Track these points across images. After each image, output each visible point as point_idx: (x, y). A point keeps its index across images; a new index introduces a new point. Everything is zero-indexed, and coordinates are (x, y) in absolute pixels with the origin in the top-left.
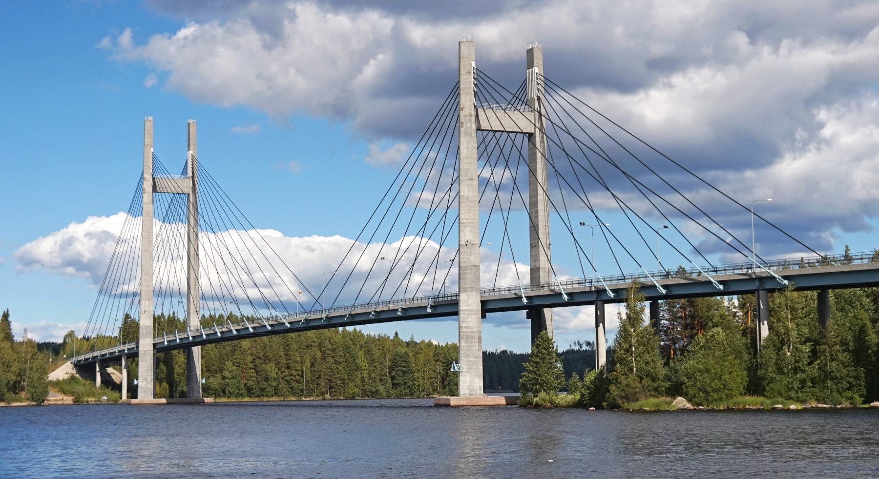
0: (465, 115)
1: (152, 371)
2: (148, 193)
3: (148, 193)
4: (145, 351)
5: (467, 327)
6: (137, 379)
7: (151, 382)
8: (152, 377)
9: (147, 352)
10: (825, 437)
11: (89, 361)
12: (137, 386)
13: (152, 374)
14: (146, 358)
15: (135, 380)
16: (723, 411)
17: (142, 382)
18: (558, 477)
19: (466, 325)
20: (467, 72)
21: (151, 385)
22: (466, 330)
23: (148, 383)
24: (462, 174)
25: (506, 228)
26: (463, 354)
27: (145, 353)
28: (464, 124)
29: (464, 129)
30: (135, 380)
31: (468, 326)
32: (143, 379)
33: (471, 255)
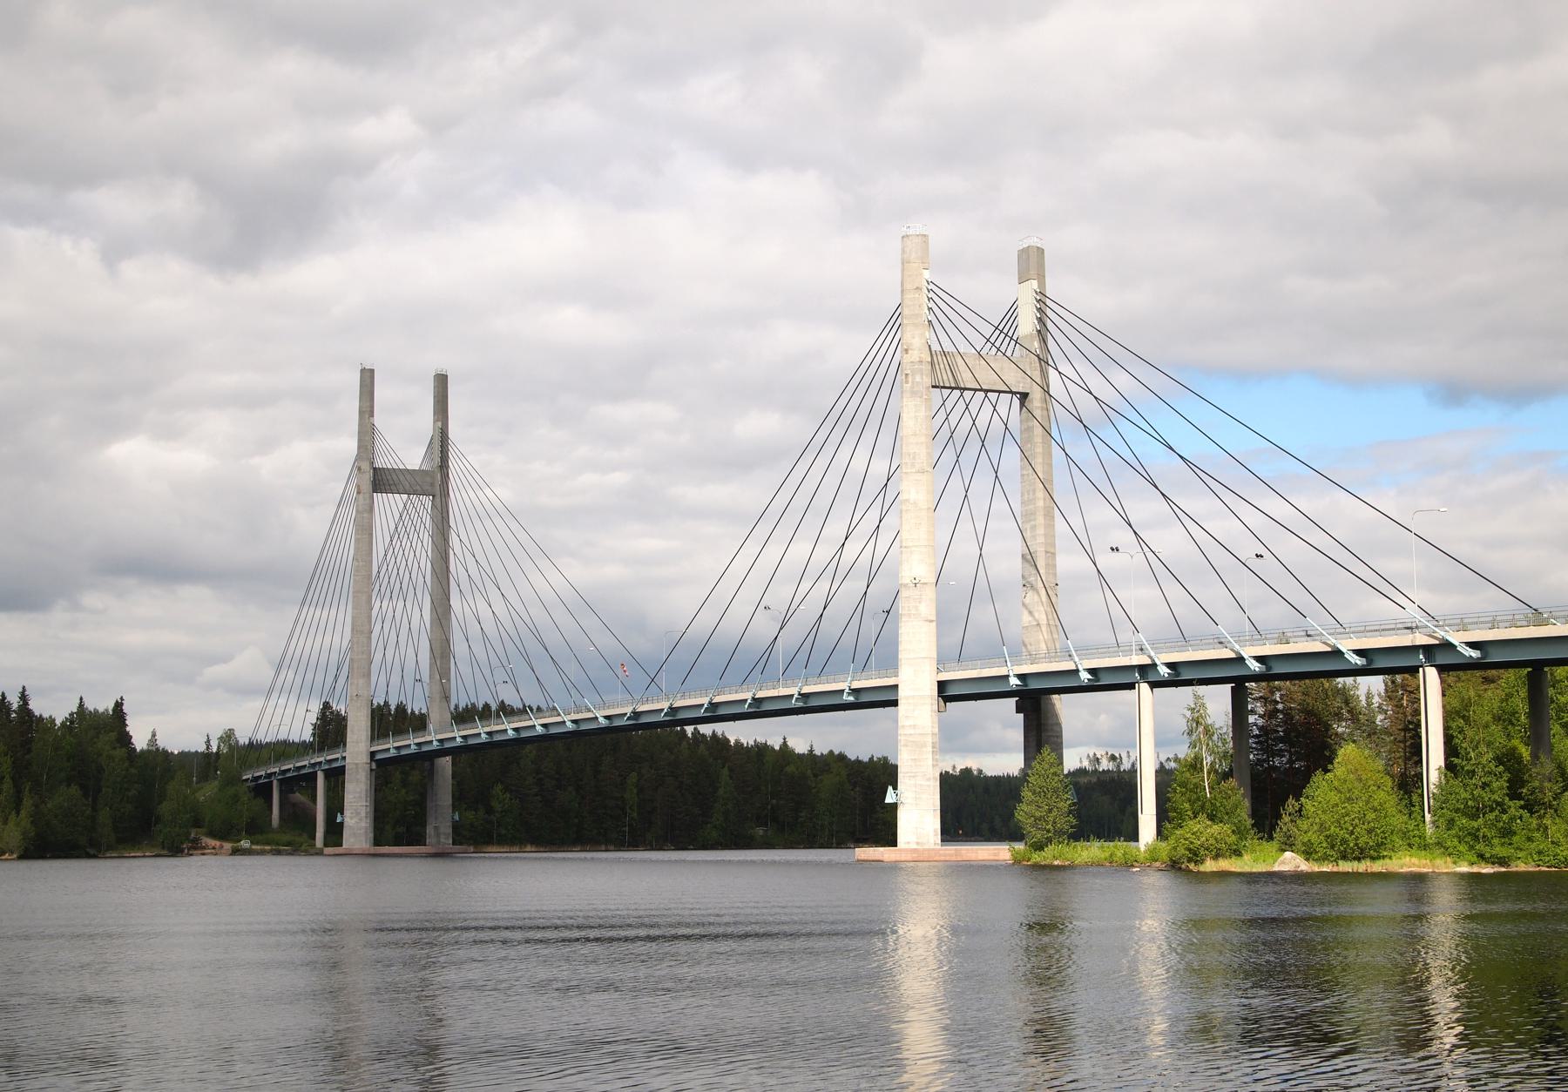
0: (912, 362)
4: (357, 764)
5: (914, 727)
9: (360, 766)
12: (894, 806)
17: (351, 818)
22: (912, 732)
23: (360, 820)
27: (357, 768)
31: (915, 725)
32: (352, 813)
33: (920, 602)
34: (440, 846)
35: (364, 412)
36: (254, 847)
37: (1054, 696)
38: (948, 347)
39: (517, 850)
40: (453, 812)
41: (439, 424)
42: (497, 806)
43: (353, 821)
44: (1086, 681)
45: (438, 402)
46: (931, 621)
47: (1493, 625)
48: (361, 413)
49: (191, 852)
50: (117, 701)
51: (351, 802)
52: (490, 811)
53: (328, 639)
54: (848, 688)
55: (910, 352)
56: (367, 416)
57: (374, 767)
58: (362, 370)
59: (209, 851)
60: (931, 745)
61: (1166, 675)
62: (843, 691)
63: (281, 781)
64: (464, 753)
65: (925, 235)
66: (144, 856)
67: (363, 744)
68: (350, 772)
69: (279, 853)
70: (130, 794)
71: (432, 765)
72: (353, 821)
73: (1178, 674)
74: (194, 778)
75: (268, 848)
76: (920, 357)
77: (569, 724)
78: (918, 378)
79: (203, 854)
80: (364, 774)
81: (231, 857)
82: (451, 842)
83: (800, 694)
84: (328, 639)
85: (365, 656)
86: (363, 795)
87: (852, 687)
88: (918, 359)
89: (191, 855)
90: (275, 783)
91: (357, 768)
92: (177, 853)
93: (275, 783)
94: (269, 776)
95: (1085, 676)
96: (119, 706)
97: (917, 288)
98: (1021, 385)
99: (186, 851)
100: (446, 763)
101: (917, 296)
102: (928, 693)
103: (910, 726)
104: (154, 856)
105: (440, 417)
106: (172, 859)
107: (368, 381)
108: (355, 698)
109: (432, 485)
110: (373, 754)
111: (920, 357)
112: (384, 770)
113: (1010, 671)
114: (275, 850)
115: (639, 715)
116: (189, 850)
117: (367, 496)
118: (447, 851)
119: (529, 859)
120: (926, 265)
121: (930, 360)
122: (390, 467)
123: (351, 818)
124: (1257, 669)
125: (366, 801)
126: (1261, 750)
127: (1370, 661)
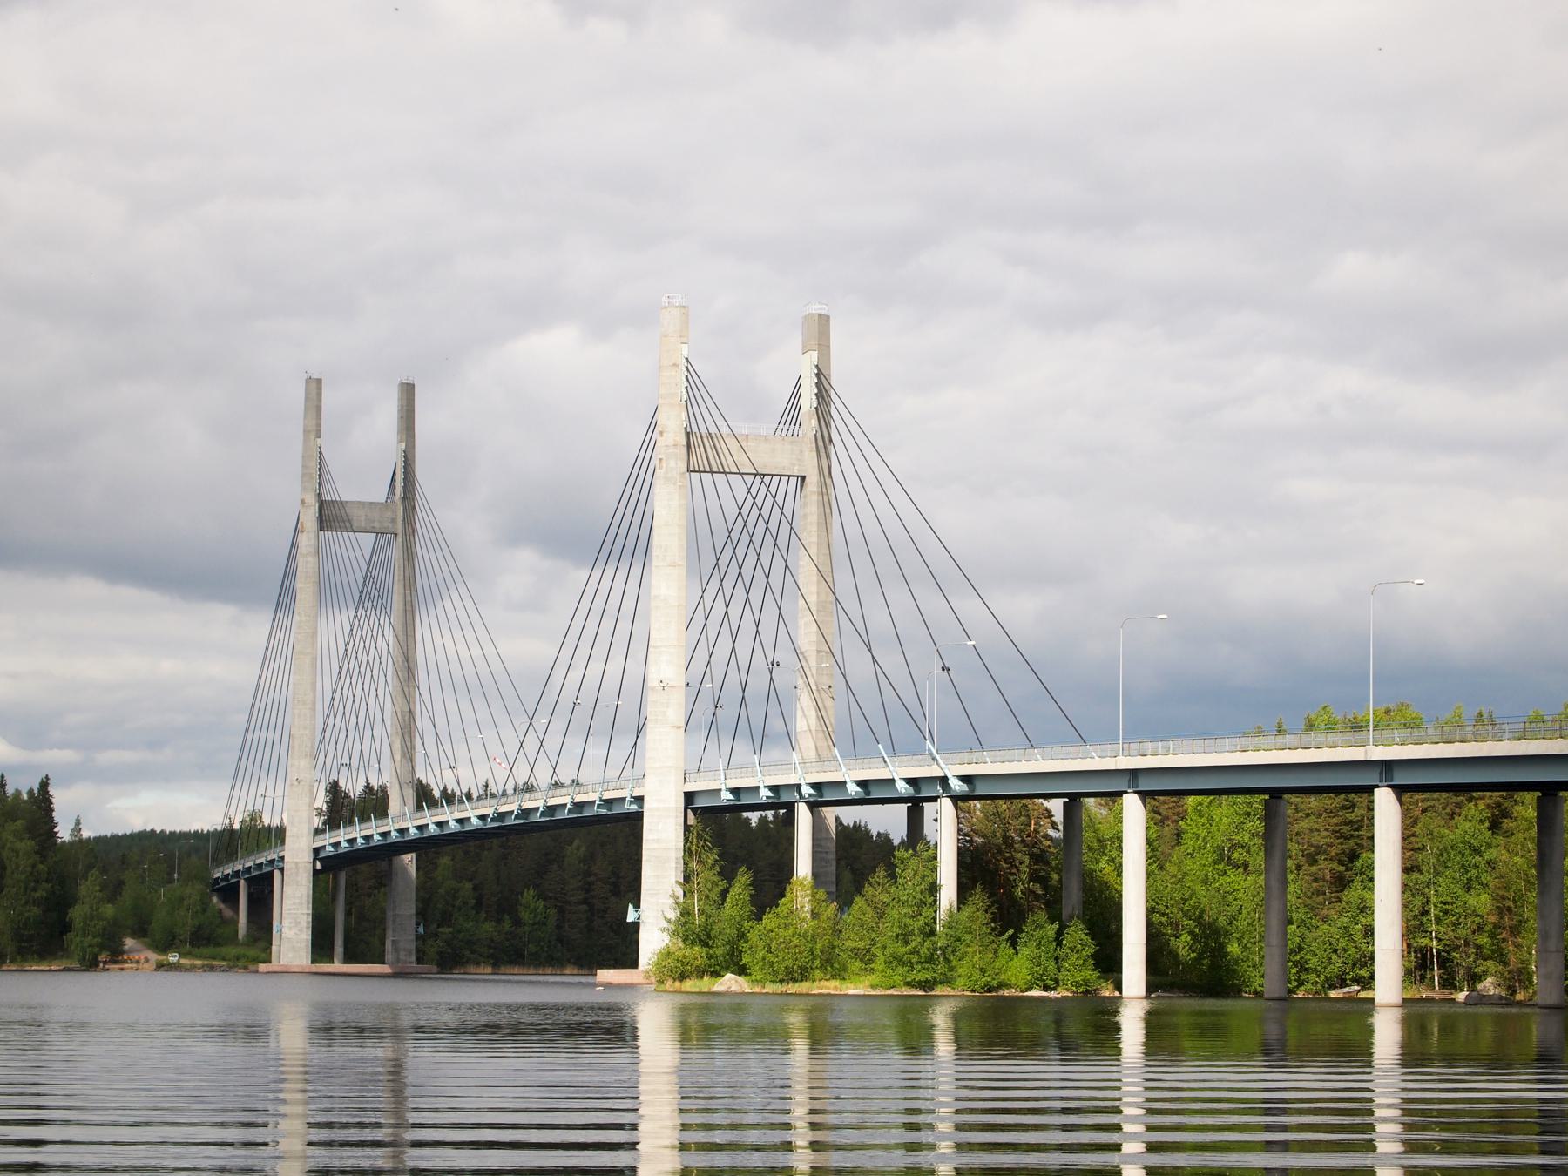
0: (667, 446)
1: (311, 906)
2: (308, 532)
3: (308, 532)
4: (297, 863)
5: (658, 841)
6: (637, 905)
7: (307, 928)
8: (310, 919)
9: (300, 865)
10: (601, 1019)
11: (508, 823)
12: (636, 926)
13: (310, 912)
14: (299, 879)
15: (631, 907)
16: (672, 992)
17: (290, 929)
18: (900, 1160)
19: (656, 837)
20: (671, 364)
21: (308, 935)
22: (656, 846)
23: (301, 931)
24: (657, 556)
25: (733, 648)
26: (647, 890)
27: (297, 868)
28: (664, 461)
29: (663, 471)
30: (631, 907)
31: (658, 839)
32: (291, 923)
33: (668, 707)
34: (400, 965)
35: (309, 432)
36: (182, 961)
37: (823, 808)
38: (713, 430)
39: (549, 972)
40: (418, 924)
41: (403, 446)
42: (525, 916)
43: (292, 932)
44: (764, 798)
45: (402, 417)
46: (680, 727)
47: (1485, 724)
48: (306, 432)
49: (107, 967)
50: (42, 781)
51: (290, 910)
52: (518, 922)
53: (596, 668)
54: (629, 796)
55: (665, 434)
56: (312, 437)
57: (319, 866)
58: (307, 380)
59: (130, 965)
60: (675, 860)
61: (853, 794)
62: (625, 798)
63: (249, 881)
64: (426, 846)
65: (684, 307)
66: (49, 971)
67: (305, 839)
68: (289, 873)
69: (212, 968)
70: (38, 894)
71: (390, 865)
72: (292, 932)
73: (868, 793)
74: (176, 875)
75: (198, 962)
76: (675, 440)
77: (453, 824)
78: (672, 463)
79: (122, 969)
80: (305, 875)
81: (155, 973)
82: (413, 958)
83: (601, 800)
84: (596, 668)
85: (307, 732)
86: (304, 900)
87: (604, 798)
88: (673, 443)
89: (108, 970)
90: (242, 883)
91: (297, 868)
92: (91, 967)
93: (242, 883)
94: (236, 874)
95: (853, 790)
96: (44, 785)
97: (675, 365)
98: (796, 468)
99: (101, 965)
100: (409, 860)
101: (673, 373)
102: (673, 804)
103: (653, 840)
104: (59, 970)
105: (404, 437)
106: (87, 974)
107: (314, 392)
108: (296, 783)
109: (394, 521)
110: (317, 851)
111: (675, 440)
112: (328, 867)
113: (846, 776)
114: (207, 965)
115: (555, 810)
116: (105, 963)
117: (312, 535)
118: (407, 971)
119: (455, 979)
120: (684, 340)
121: (685, 443)
122: (334, 499)
123: (290, 929)
124: (903, 791)
125: (308, 909)
126: (1232, 868)
127: (868, 793)
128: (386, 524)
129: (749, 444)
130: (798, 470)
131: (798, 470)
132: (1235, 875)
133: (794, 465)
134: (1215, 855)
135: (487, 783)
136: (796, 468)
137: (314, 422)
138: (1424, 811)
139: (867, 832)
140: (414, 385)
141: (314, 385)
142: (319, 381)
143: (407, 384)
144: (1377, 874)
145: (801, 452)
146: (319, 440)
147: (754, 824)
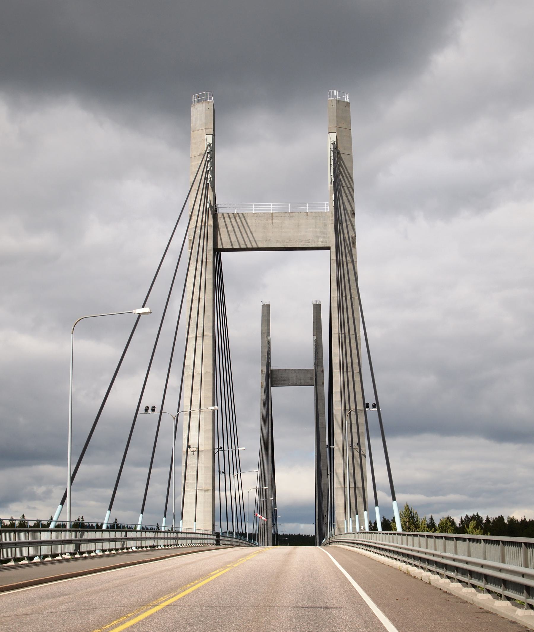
35: (264, 333)
48: (263, 333)
56: (265, 336)
98: (321, 240)
128: (308, 381)
129: (274, 221)
130: (322, 242)
131: (322, 242)
132: (275, 567)
133: (318, 237)
134: (443, 521)
135: (431, 517)
136: (321, 240)
137: (266, 328)
138: (297, 240)
139: (302, 535)
140: (320, 305)
141: (266, 308)
142: (268, 306)
143: (316, 304)
144: (455, 534)
145: (325, 225)
146: (269, 337)
147: (507, 523)
